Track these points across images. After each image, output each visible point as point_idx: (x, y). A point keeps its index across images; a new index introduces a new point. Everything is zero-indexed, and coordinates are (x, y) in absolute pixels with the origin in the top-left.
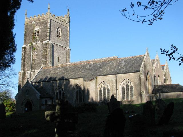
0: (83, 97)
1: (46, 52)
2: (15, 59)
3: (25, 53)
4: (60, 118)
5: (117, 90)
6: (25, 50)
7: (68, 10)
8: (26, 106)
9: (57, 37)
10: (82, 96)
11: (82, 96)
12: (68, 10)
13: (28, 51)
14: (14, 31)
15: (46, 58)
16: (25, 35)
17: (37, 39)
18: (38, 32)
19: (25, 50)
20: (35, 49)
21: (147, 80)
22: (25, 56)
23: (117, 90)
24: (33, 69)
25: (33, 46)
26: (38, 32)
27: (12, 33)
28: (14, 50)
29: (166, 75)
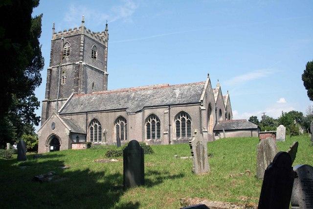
0: (126, 134)
1: (78, 76)
2: (41, 79)
3: (50, 76)
4: (31, 118)
5: (170, 125)
6: (51, 73)
7: (107, 25)
8: (51, 144)
9: (92, 57)
10: (125, 133)
11: (125, 133)
12: (107, 25)
13: (54, 74)
14: (40, 40)
15: (77, 83)
16: (51, 54)
17: (67, 59)
18: (69, 51)
19: (51, 73)
20: (64, 72)
21: (216, 112)
22: (50, 80)
23: (170, 125)
24: (60, 96)
25: (61, 69)
26: (69, 51)
27: (39, 43)
28: (40, 66)
29: (228, 110)
